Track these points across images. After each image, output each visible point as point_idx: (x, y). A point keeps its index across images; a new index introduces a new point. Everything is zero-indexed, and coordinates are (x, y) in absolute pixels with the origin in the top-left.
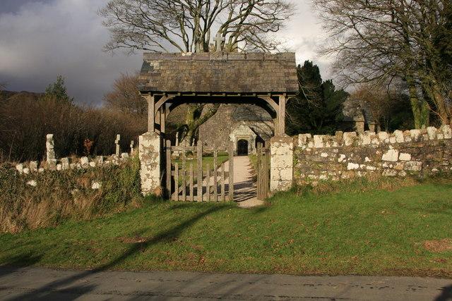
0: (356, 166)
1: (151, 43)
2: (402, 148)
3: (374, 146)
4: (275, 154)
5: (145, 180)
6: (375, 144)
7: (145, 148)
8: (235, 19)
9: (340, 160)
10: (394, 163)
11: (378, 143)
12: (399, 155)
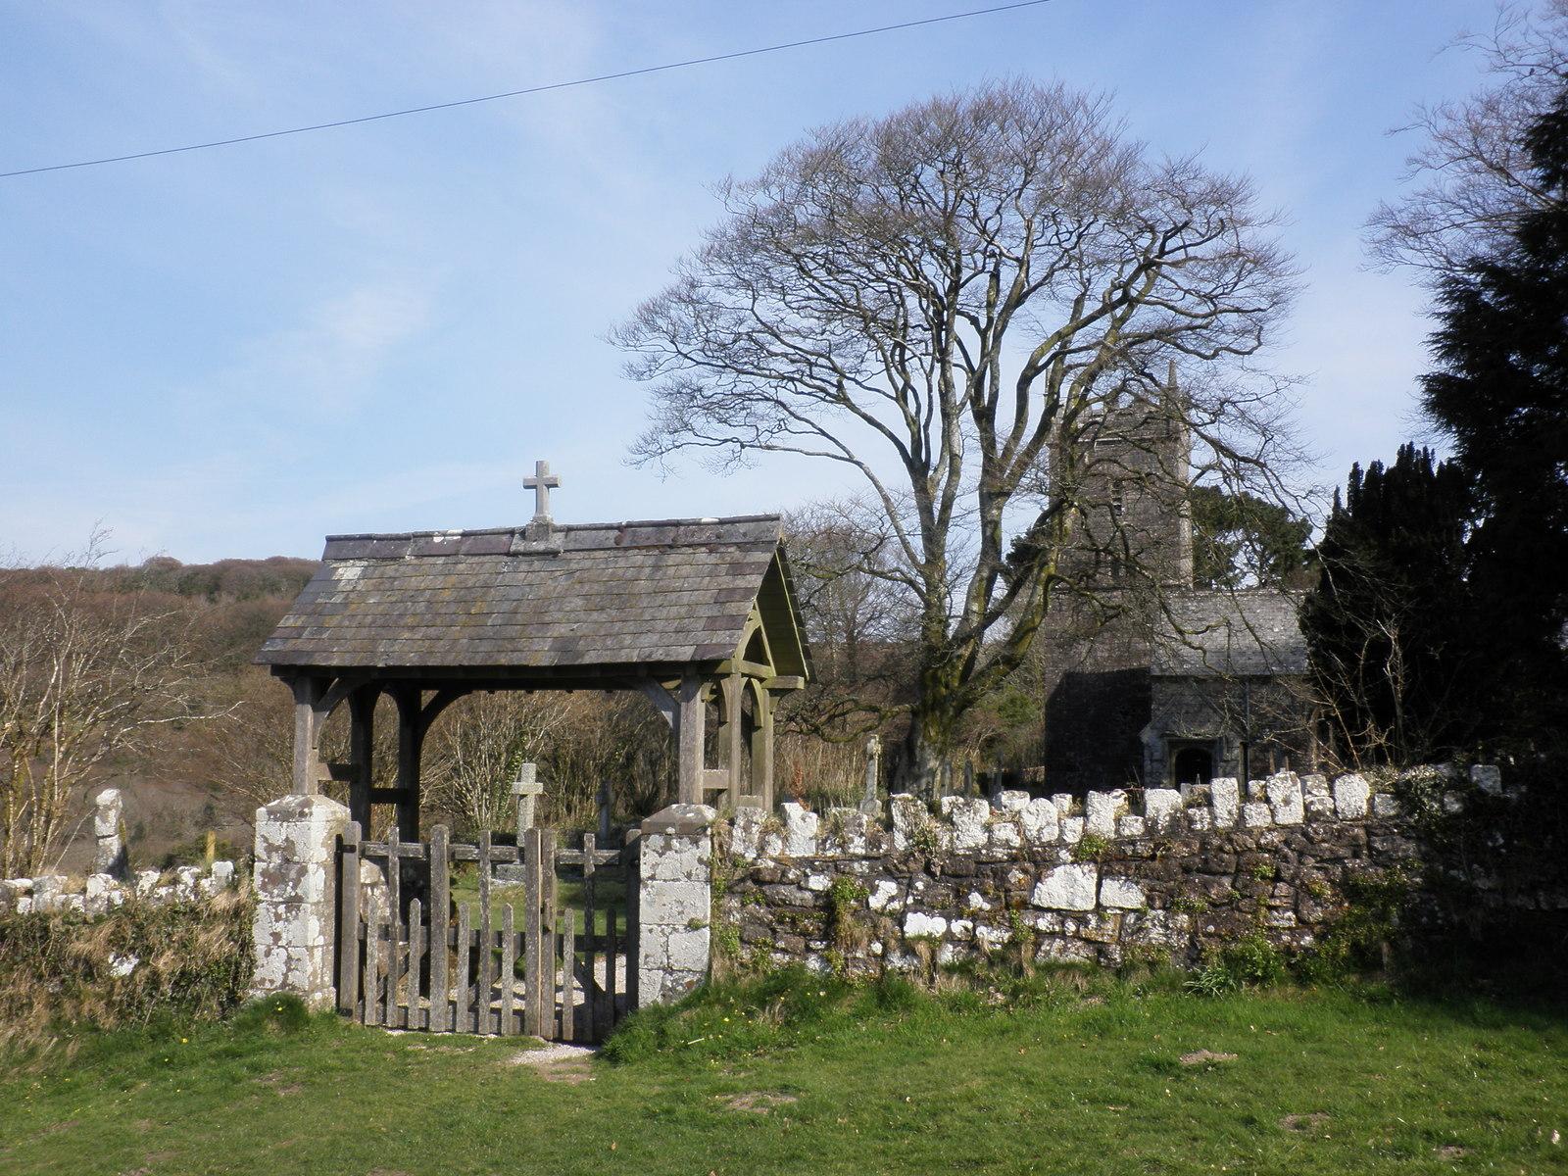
0: (937, 925)
1: (795, 425)
2: (1108, 859)
3: (1000, 853)
4: (653, 878)
5: (268, 954)
6: (1007, 844)
7: (271, 848)
8: (1092, 318)
9: (876, 902)
10: (1081, 918)
11: (1017, 842)
12: (1099, 885)
